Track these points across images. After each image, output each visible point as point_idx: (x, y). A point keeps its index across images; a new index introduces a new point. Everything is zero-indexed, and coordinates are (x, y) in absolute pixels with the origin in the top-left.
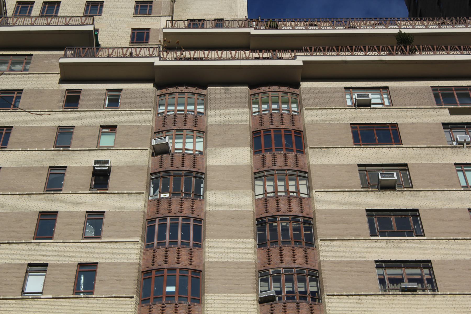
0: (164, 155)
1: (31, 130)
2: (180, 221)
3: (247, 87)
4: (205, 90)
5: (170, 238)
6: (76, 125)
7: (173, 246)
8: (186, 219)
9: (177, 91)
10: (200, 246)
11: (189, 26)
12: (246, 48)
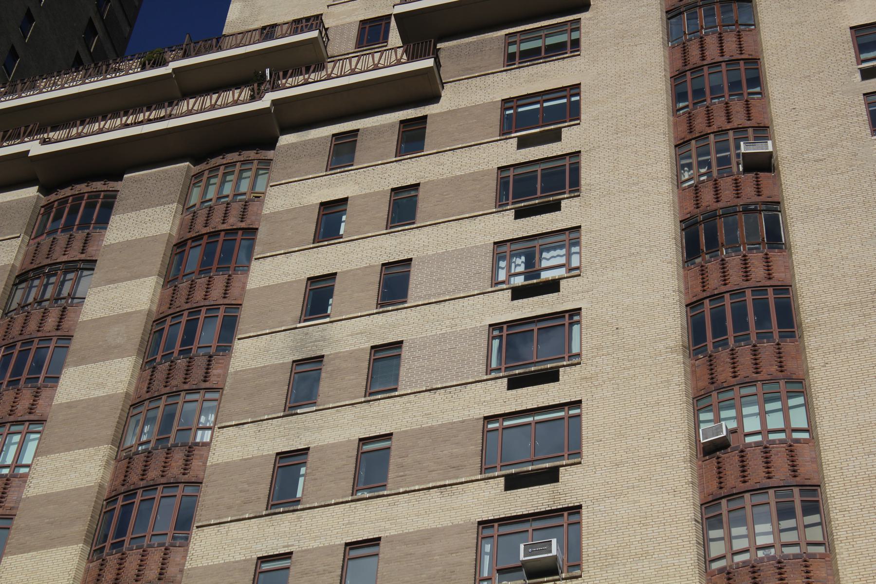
0: (761, 174)
1: (456, 183)
2: (749, 296)
3: (188, 163)
4: (272, 152)
5: (780, 326)
6: (422, 181)
7: (743, 344)
8: (759, 290)
9: (225, 161)
10: (792, 335)
11: (296, 32)
12: (188, 94)
